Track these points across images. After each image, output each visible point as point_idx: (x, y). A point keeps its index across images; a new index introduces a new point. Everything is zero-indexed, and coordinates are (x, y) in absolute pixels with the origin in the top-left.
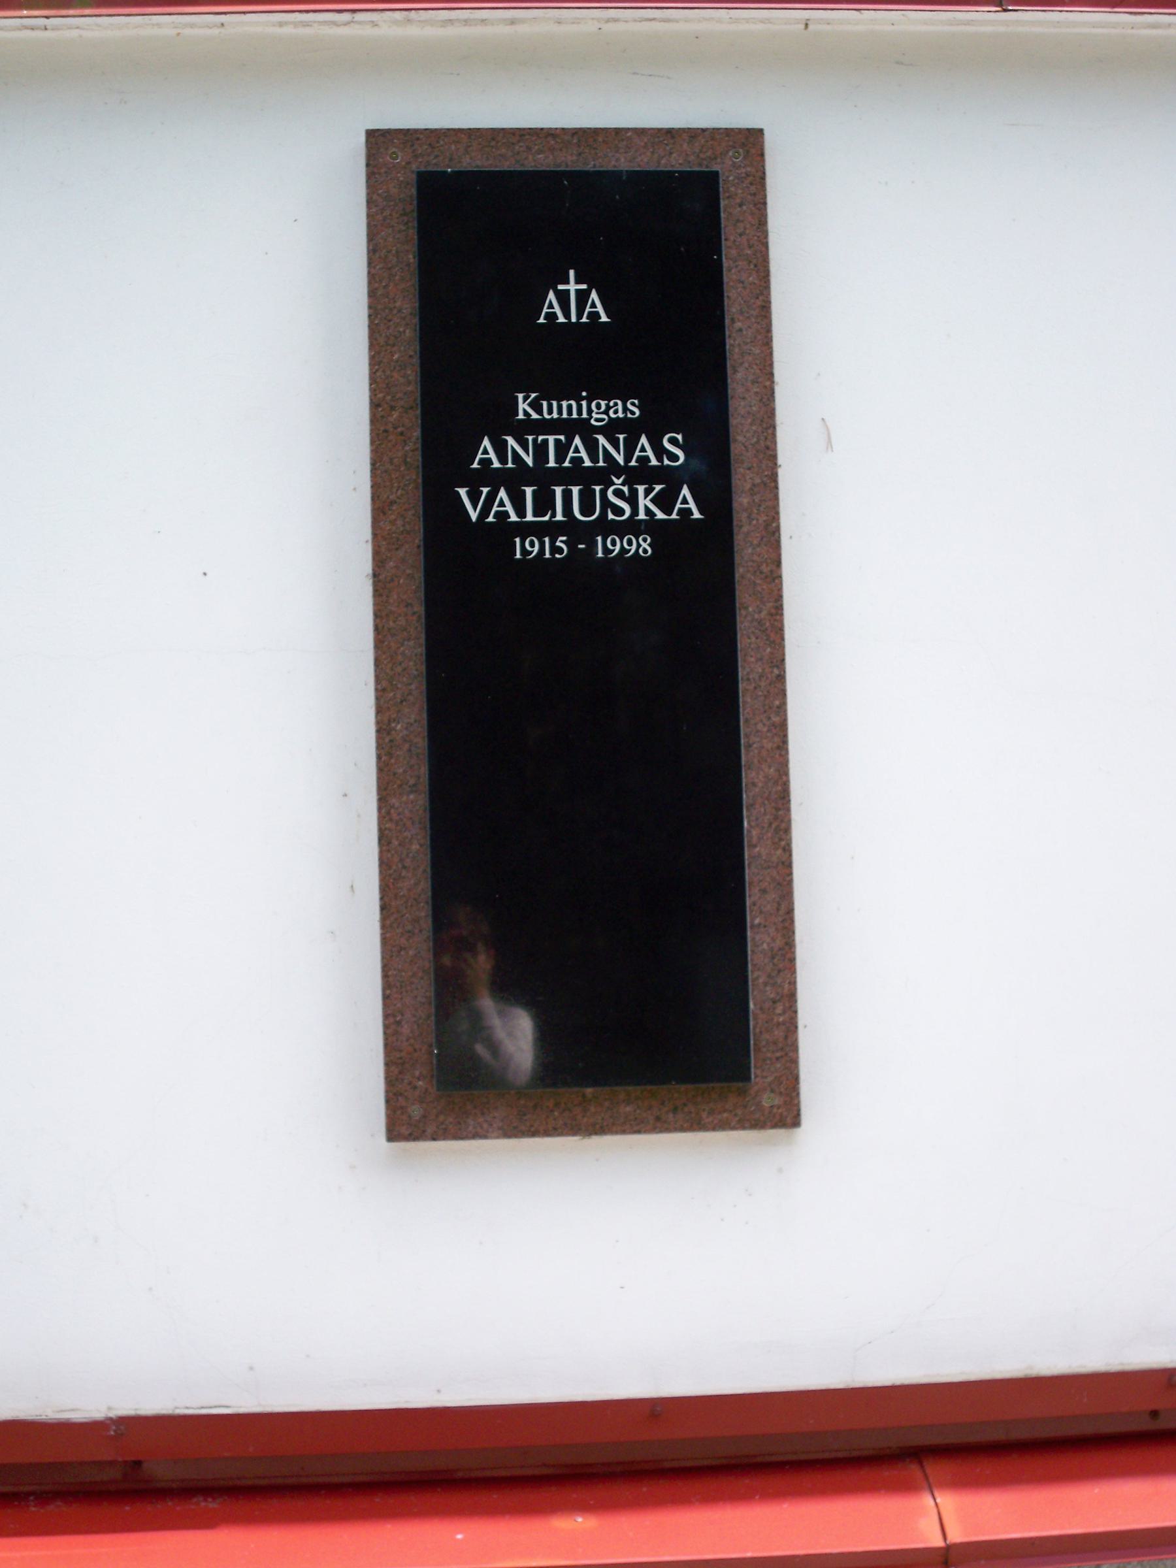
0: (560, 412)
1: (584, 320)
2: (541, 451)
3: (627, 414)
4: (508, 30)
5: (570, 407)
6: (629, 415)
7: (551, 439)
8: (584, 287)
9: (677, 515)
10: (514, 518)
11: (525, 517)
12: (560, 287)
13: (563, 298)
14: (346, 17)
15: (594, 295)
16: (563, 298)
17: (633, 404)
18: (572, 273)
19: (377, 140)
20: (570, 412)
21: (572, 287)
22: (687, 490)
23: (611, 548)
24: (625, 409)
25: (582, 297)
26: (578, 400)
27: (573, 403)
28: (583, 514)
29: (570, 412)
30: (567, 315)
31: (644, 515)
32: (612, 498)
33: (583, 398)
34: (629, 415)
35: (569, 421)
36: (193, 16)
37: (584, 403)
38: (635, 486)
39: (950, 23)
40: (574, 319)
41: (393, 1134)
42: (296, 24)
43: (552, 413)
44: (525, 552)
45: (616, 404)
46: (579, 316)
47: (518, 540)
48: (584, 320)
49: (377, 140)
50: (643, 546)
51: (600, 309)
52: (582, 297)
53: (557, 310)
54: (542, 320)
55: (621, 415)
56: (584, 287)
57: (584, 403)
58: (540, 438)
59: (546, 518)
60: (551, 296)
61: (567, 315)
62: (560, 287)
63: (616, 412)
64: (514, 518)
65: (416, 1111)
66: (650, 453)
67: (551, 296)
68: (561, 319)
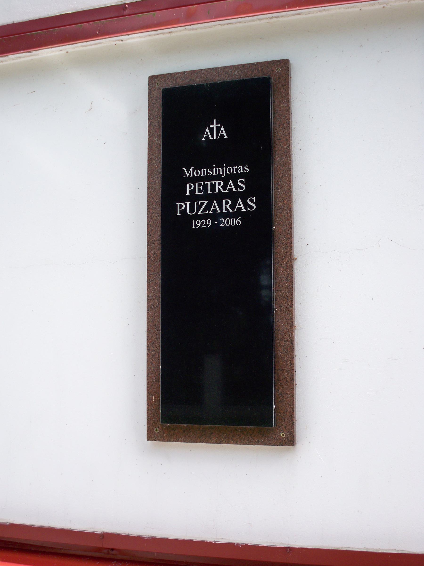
0: (216, 173)
1: (219, 138)
2: (205, 187)
3: (244, 171)
4: (169, 35)
5: (219, 170)
6: (245, 172)
7: (209, 183)
8: (219, 125)
9: (236, 210)
10: (219, 211)
11: (223, 211)
12: (210, 126)
13: (211, 130)
14: (182, 28)
15: (222, 128)
16: (211, 130)
17: (246, 167)
18: (215, 120)
19: (152, 79)
20: (204, 174)
21: (215, 126)
22: (207, 202)
23: (197, 224)
24: (244, 169)
25: (218, 129)
26: (222, 167)
27: (221, 168)
28: (190, 212)
29: (204, 174)
30: (213, 136)
31: (179, 214)
32: (249, 202)
33: (224, 167)
34: (245, 172)
35: (216, 176)
36: (226, 21)
37: (224, 168)
38: (222, 200)
39: (74, 48)
40: (215, 138)
41: (149, 438)
42: (201, 28)
43: (241, 171)
44: (196, 226)
45: (240, 168)
46: (217, 136)
47: (193, 221)
48: (219, 138)
49: (152, 79)
50: (237, 222)
51: (224, 133)
52: (218, 129)
53: (209, 135)
54: (204, 139)
55: (242, 172)
56: (219, 125)
57: (224, 168)
58: (205, 183)
59: (207, 212)
60: (207, 130)
61: (213, 136)
62: (210, 126)
63: (240, 171)
64: (219, 211)
65: (283, 435)
66: (233, 187)
67: (207, 130)
68: (211, 138)
